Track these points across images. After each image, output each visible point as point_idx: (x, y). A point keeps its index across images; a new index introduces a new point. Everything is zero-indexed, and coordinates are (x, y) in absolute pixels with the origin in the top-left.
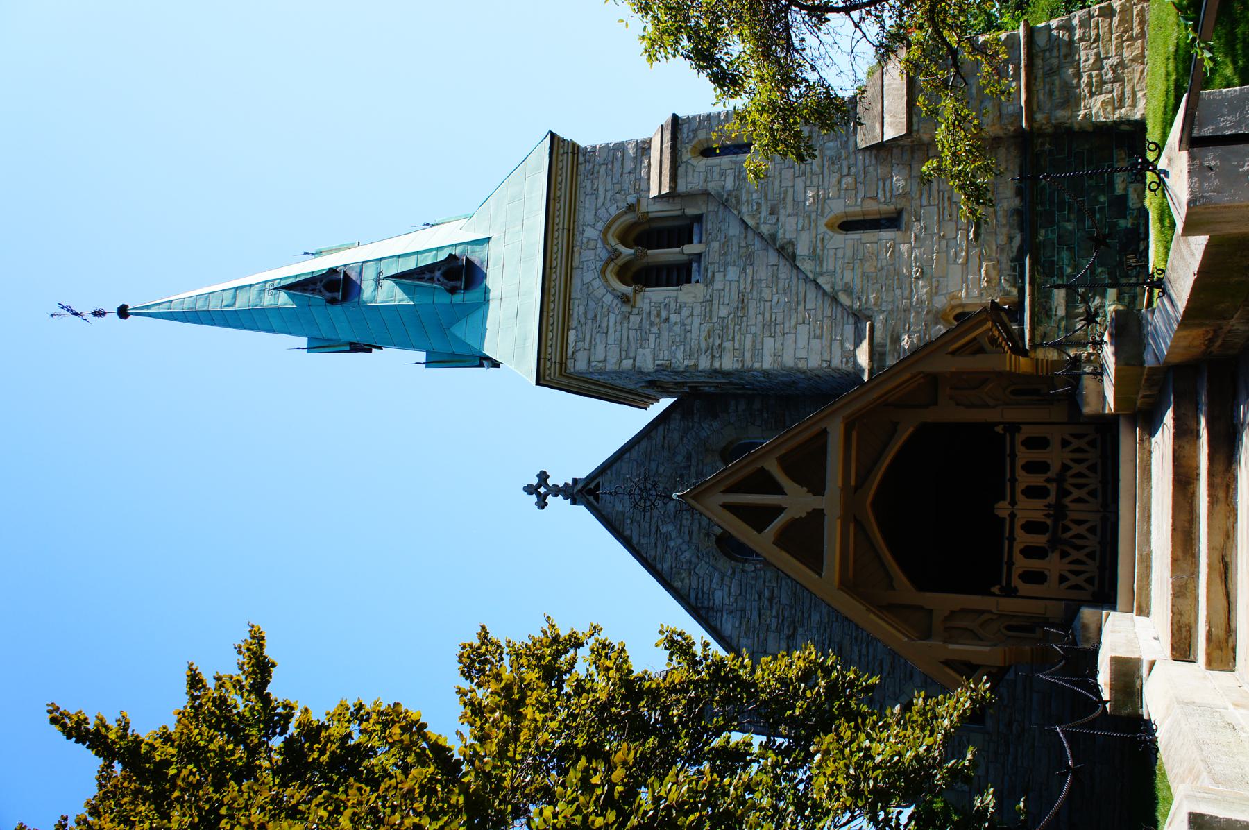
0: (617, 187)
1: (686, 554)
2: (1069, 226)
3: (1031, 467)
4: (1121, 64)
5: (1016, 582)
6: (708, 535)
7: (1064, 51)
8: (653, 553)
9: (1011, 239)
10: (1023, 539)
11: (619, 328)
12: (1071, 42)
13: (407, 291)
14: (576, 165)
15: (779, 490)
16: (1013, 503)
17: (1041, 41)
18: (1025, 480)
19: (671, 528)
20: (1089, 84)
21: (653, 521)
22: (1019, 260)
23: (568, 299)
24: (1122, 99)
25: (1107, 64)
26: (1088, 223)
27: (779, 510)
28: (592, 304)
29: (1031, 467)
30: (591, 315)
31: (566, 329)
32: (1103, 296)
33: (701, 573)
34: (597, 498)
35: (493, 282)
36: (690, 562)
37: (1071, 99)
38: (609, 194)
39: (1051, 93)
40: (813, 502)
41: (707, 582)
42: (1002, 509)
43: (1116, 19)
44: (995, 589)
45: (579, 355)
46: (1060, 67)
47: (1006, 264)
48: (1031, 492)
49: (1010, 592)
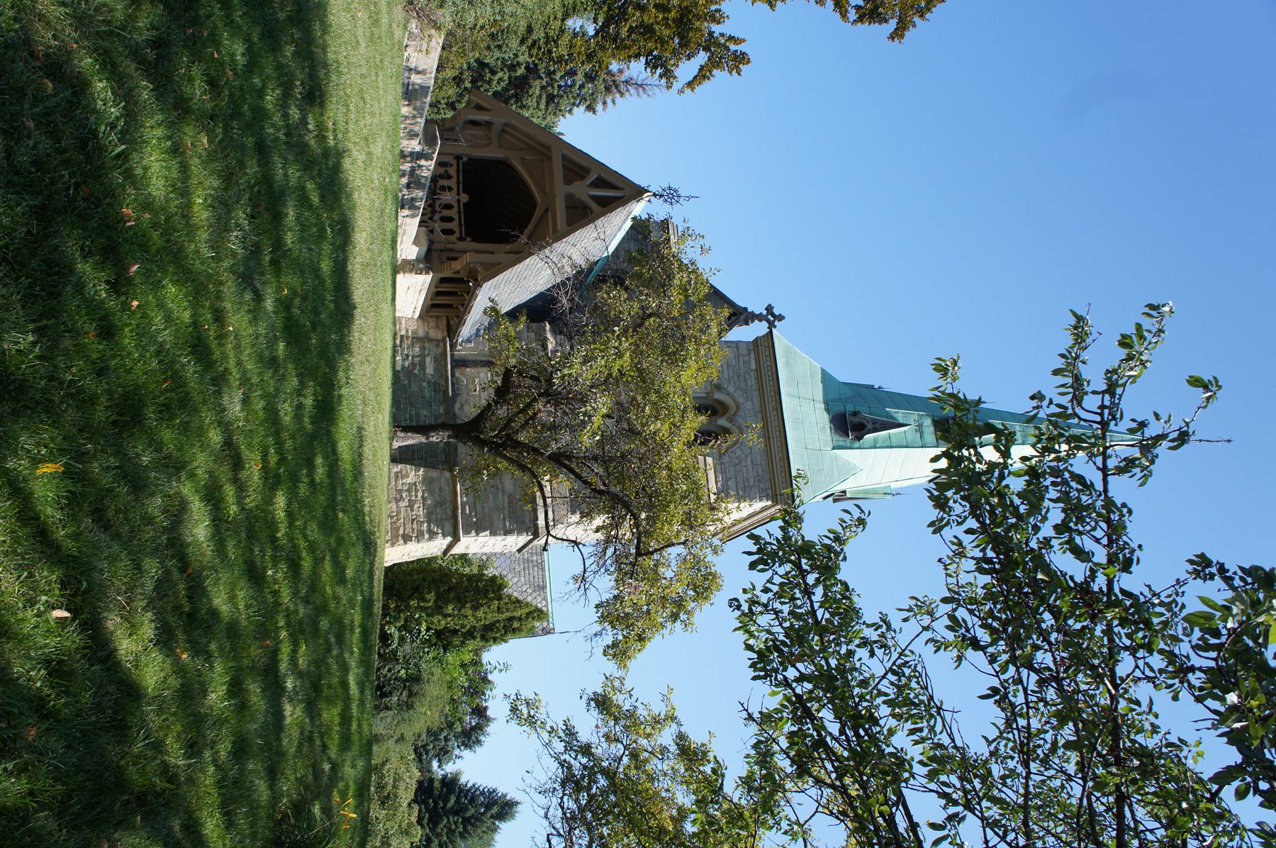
0: (738, 468)
3: (450, 219)
4: (397, 501)
5: (454, 162)
7: (433, 517)
9: (461, 408)
10: (452, 183)
12: (429, 522)
13: (889, 416)
14: (773, 486)
16: (459, 201)
17: (448, 526)
18: (453, 213)
20: (417, 491)
22: (455, 395)
23: (761, 389)
24: (397, 477)
25: (406, 503)
26: (413, 412)
28: (742, 385)
29: (450, 219)
31: (759, 369)
32: (403, 366)
35: (824, 419)
37: (428, 482)
39: (440, 490)
42: (465, 198)
43: (401, 532)
45: (746, 352)
46: (435, 506)
47: (463, 392)
48: (449, 207)
49: (458, 158)
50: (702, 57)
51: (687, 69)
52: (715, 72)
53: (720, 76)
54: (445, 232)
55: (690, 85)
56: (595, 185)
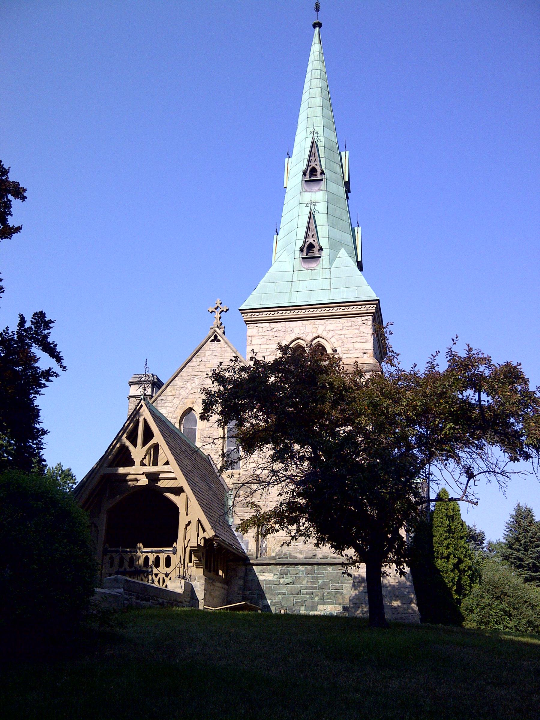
1: (184, 392)
2: (304, 582)
3: (157, 559)
6: (193, 403)
8: (184, 375)
11: (268, 350)
15: (144, 444)
19: (197, 383)
21: (200, 373)
27: (135, 446)
29: (157, 559)
30: (276, 334)
33: (174, 401)
34: (212, 341)
36: (180, 395)
38: (342, 336)
40: (137, 461)
41: (170, 404)
44: (107, 545)
49: (105, 552)
50: (36, 350)
51: (44, 362)
52: (50, 340)
53: (54, 336)
54: (168, 564)
55: (59, 359)
56: (133, 439)
